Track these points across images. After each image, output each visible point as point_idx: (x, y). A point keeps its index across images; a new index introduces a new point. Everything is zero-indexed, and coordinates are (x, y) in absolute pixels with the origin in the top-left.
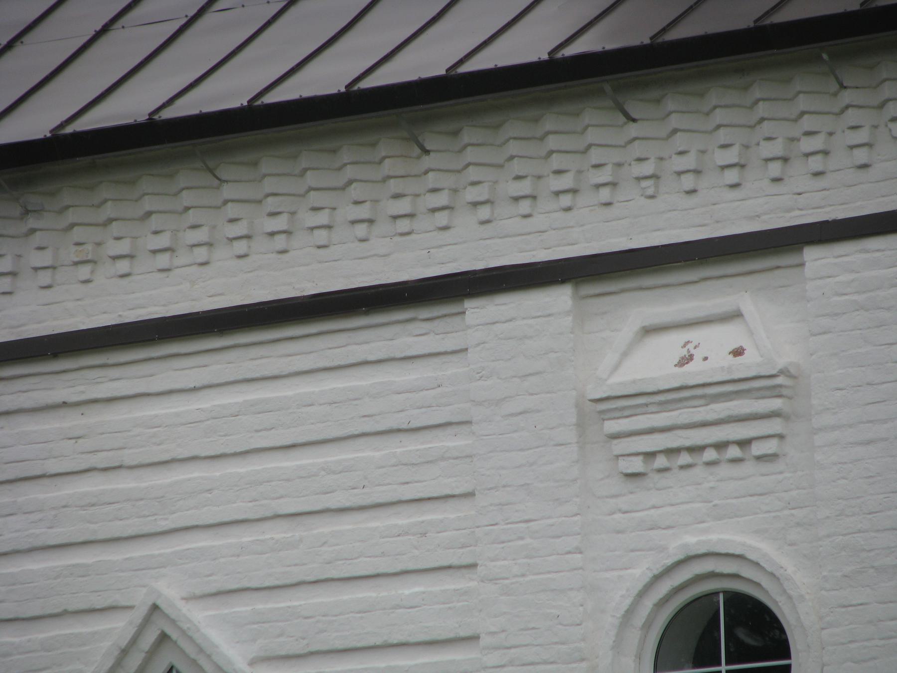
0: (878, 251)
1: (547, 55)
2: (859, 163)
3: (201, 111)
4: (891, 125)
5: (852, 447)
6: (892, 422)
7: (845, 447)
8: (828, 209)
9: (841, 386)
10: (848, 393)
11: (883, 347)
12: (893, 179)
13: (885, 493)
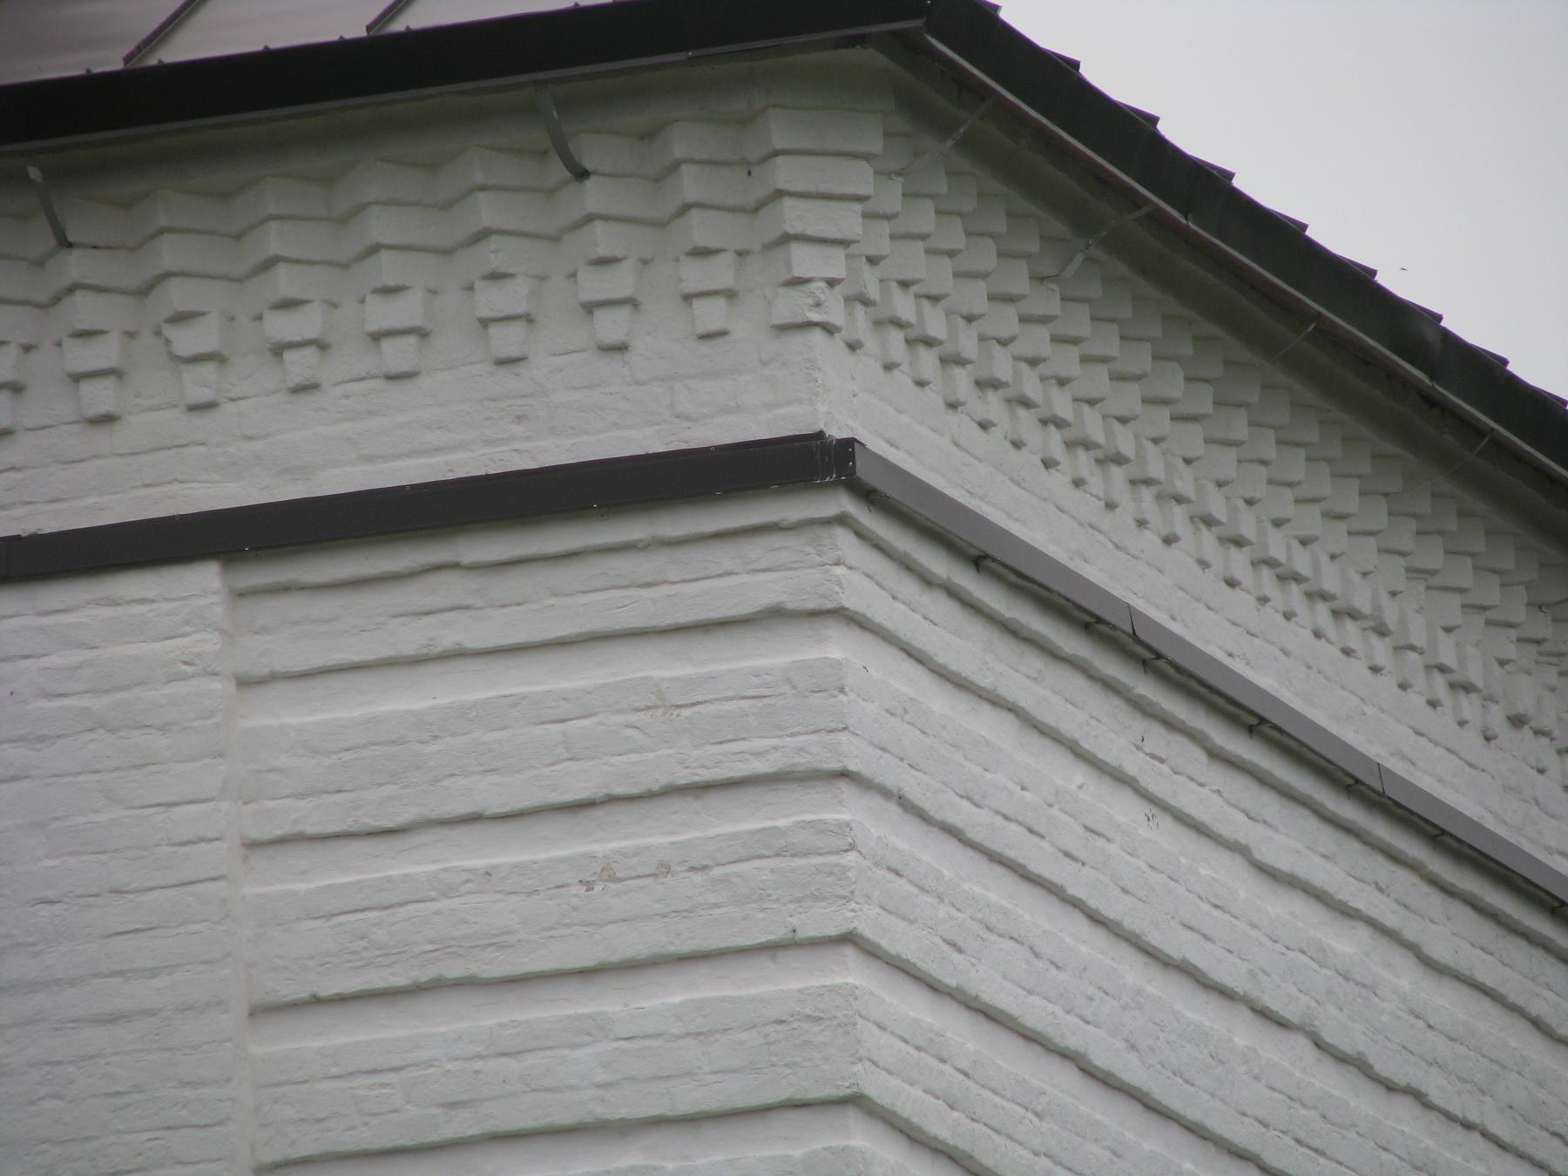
0: (141, 601)
1: (365, 29)
2: (91, 412)
3: (88, 71)
4: (168, 331)
5: (73, 1028)
6: (169, 974)
7: (57, 1029)
8: (19, 511)
9: (50, 894)
10: (67, 910)
11: (148, 811)
12: (169, 448)
13: (148, 1130)
